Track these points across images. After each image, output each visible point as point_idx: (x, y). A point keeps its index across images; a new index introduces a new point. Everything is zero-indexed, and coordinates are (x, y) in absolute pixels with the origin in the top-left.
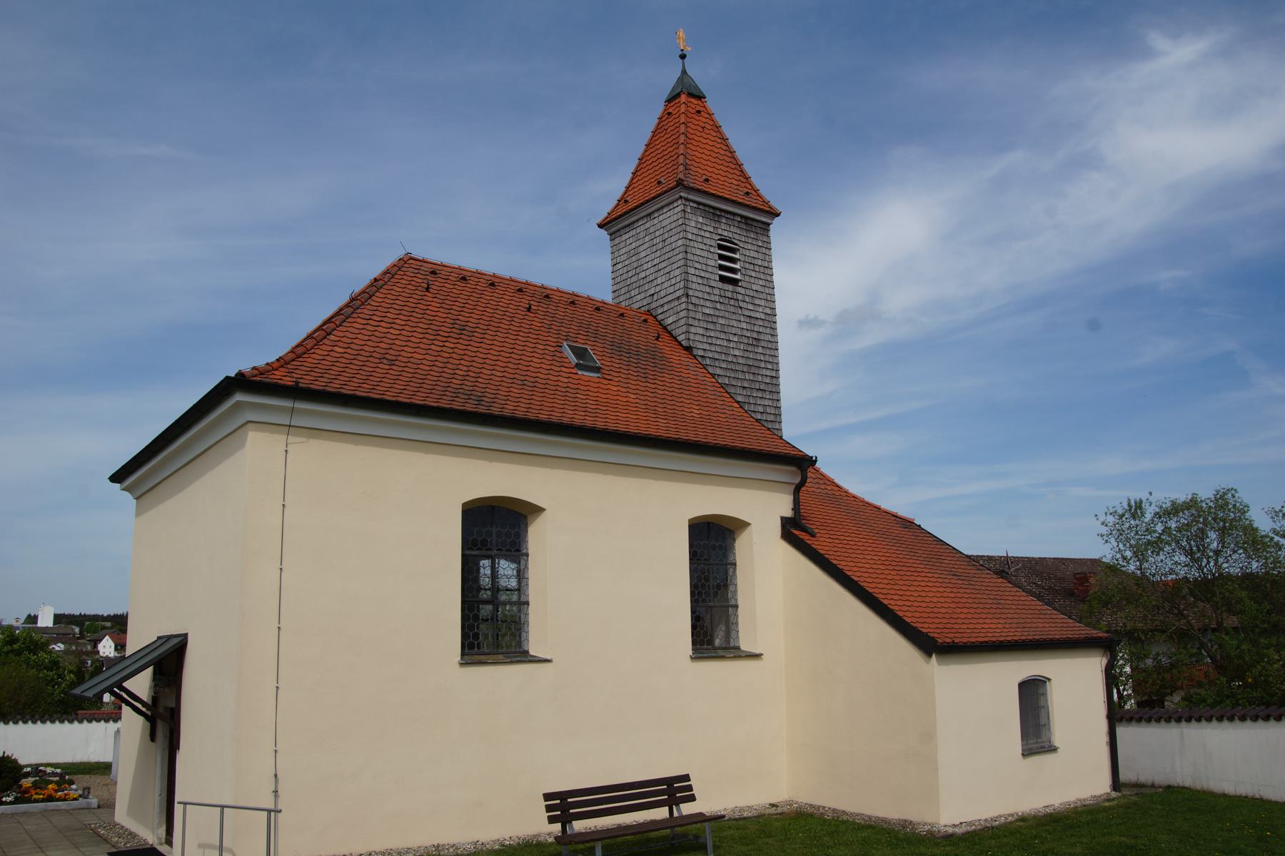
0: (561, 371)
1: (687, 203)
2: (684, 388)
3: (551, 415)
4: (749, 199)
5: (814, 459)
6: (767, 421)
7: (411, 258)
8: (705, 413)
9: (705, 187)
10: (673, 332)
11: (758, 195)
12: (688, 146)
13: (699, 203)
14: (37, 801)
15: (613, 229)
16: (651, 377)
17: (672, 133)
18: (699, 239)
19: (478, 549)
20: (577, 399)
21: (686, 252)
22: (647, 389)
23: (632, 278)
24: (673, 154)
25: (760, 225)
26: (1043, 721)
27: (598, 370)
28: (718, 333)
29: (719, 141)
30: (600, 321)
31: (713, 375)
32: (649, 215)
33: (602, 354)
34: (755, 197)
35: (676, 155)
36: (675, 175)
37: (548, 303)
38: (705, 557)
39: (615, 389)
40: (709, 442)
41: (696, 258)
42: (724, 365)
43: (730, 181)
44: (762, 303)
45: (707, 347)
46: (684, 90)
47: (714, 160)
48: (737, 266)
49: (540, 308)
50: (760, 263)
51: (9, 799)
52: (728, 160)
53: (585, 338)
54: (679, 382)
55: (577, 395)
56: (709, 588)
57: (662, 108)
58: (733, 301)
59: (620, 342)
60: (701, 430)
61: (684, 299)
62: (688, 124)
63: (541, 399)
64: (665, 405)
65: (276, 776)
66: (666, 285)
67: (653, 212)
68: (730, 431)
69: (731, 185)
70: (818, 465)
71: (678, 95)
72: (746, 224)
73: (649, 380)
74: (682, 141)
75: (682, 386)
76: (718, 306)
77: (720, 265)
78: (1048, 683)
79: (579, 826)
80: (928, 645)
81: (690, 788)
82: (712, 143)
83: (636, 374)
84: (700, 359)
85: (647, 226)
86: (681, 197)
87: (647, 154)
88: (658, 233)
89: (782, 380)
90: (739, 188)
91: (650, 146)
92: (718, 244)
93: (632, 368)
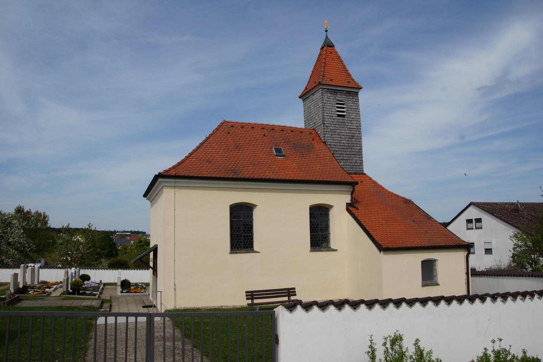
1: (323, 90)
7: (225, 122)
13: (328, 89)
14: (132, 292)
15: (303, 99)
18: (329, 102)
19: (236, 218)
21: (323, 108)
25: (354, 93)
26: (435, 275)
27: (284, 156)
32: (313, 94)
38: (318, 217)
41: (327, 109)
46: (325, 45)
50: (354, 107)
51: (125, 292)
56: (319, 228)
61: (323, 125)
65: (175, 284)
67: (314, 93)
72: (348, 93)
76: (336, 126)
77: (337, 115)
78: (437, 261)
79: (256, 301)
80: (382, 248)
81: (295, 292)
85: (312, 98)
86: (321, 88)
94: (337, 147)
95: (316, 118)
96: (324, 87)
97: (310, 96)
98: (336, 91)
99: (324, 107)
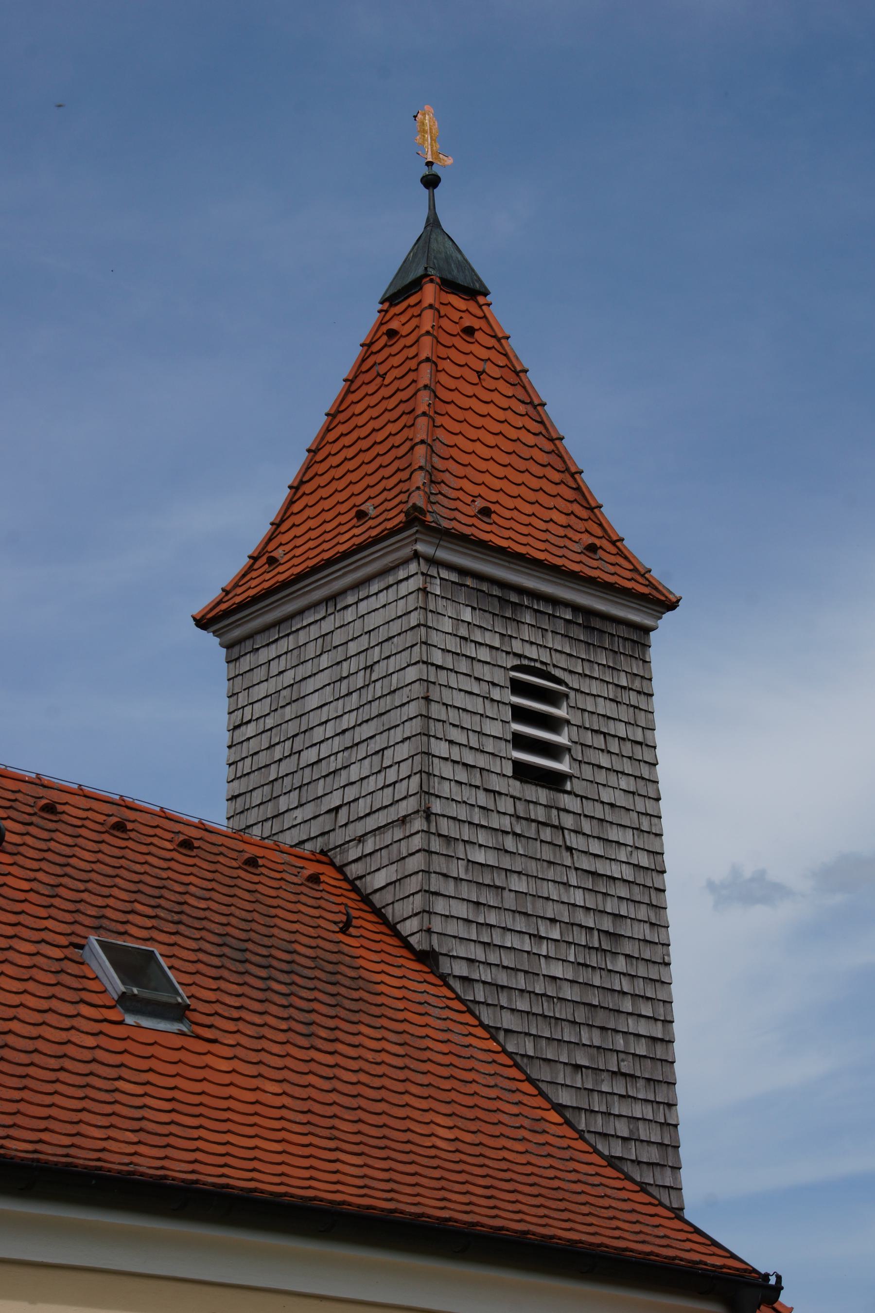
0: (78, 1015)
1: (433, 571)
2: (413, 1065)
3: (40, 1141)
4: (595, 564)
5: (773, 1281)
6: (640, 1163)
8: (469, 1138)
9: (481, 531)
10: (389, 912)
11: (621, 553)
12: (439, 420)
13: (463, 572)
15: (237, 633)
16: (323, 1033)
17: (396, 385)
18: (463, 666)
20: (118, 1096)
21: (427, 699)
22: (313, 1067)
23: (283, 764)
24: (397, 440)
25: (623, 631)
27: (179, 1012)
28: (509, 915)
29: (521, 409)
30: (192, 879)
31: (492, 1032)
32: (333, 598)
33: (191, 968)
34: (612, 559)
35: (408, 445)
36: (403, 497)
37: (51, 826)
39: (225, 1066)
40: (477, 1224)
41: (453, 716)
42: (522, 1004)
43: (547, 515)
44: (627, 837)
45: (478, 953)
46: (431, 271)
47: (505, 459)
48: (562, 739)
49: (29, 840)
50: (621, 730)
52: (544, 458)
53: (149, 923)
54: (400, 1050)
55: (120, 1084)
57: (373, 317)
58: (548, 830)
59: (243, 935)
60: (457, 1188)
61: (418, 824)
62: (439, 361)
63: (17, 1095)
64: (360, 1114)
66: (371, 784)
67: (343, 592)
68: (535, 1190)
69: (551, 526)
70: (784, 1298)
71: (416, 285)
72: (588, 628)
73: (319, 1043)
74: (422, 408)
75: (407, 1061)
76: (510, 843)
77: (518, 765)
82: (500, 415)
83: (284, 1025)
84: (457, 985)
85: (327, 626)
86: (416, 555)
87: (331, 437)
88: (353, 648)
89: (679, 1048)
90: (570, 533)
91: (342, 417)
92: (513, 681)
93: (274, 1009)
94: (510, 999)
95: (354, 773)
96: (442, 554)
97: (301, 612)
98: (514, 598)
99: (434, 694)
